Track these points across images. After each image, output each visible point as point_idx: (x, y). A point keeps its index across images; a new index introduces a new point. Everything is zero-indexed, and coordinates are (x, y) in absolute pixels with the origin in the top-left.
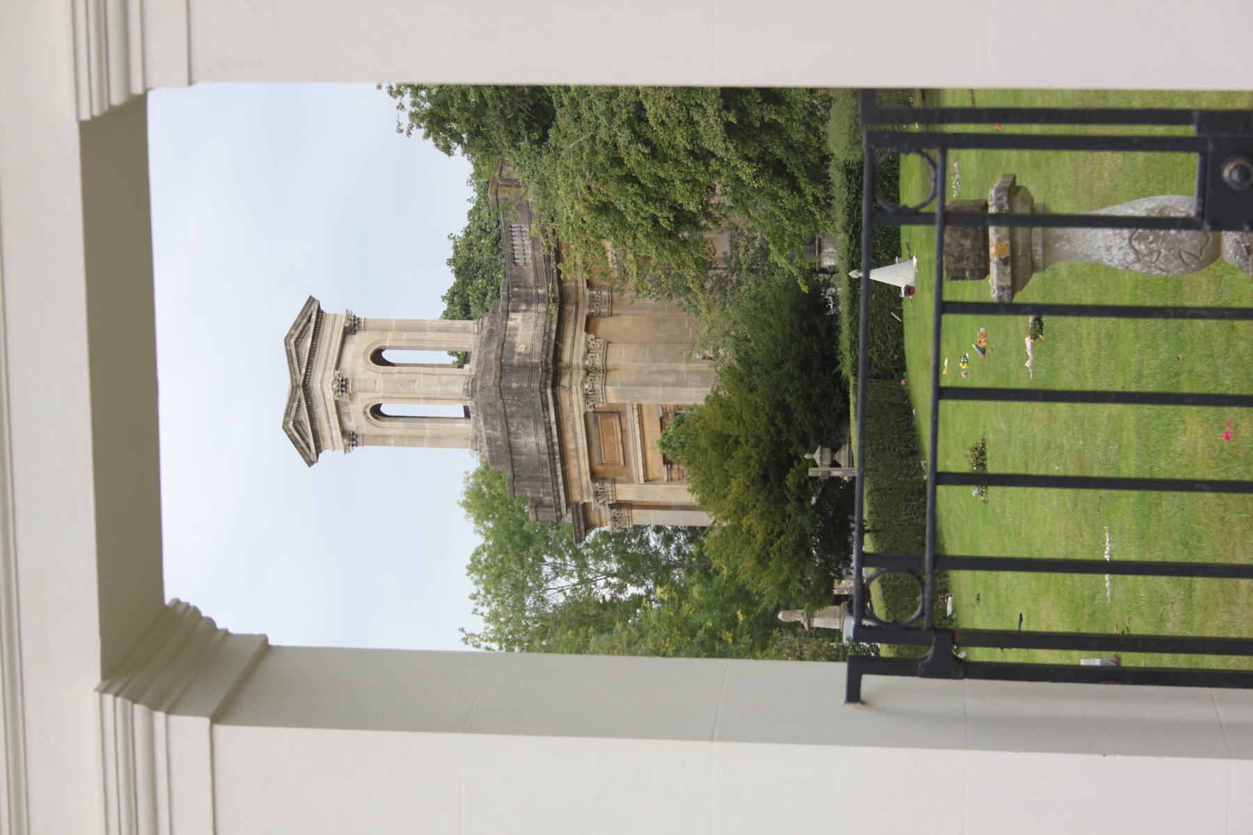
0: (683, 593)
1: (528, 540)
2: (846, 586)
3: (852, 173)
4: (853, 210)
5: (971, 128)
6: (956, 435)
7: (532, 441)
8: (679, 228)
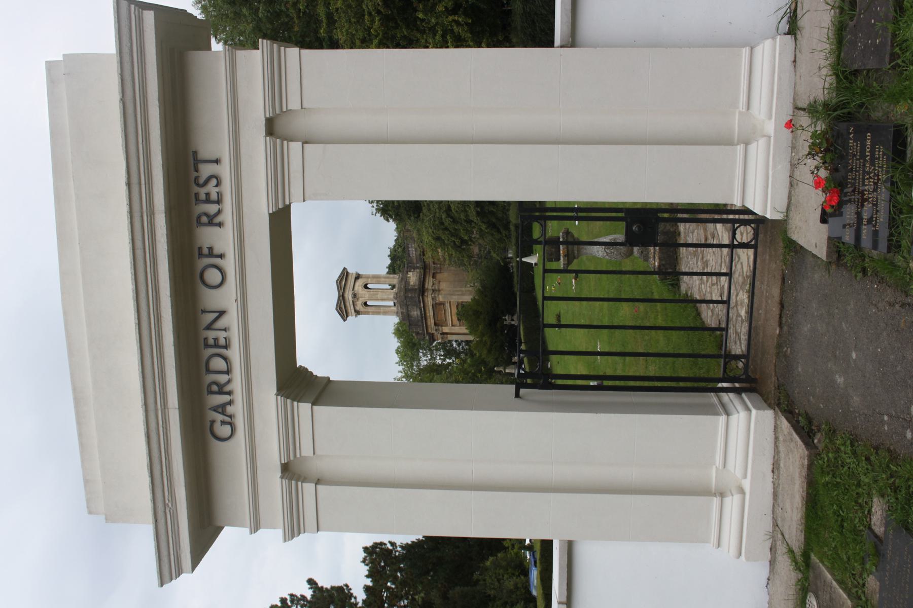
0: (464, 361)
1: (414, 344)
2: (516, 359)
3: (517, 227)
4: (517, 239)
5: (555, 214)
6: (550, 312)
7: (415, 313)
8: (462, 245)
